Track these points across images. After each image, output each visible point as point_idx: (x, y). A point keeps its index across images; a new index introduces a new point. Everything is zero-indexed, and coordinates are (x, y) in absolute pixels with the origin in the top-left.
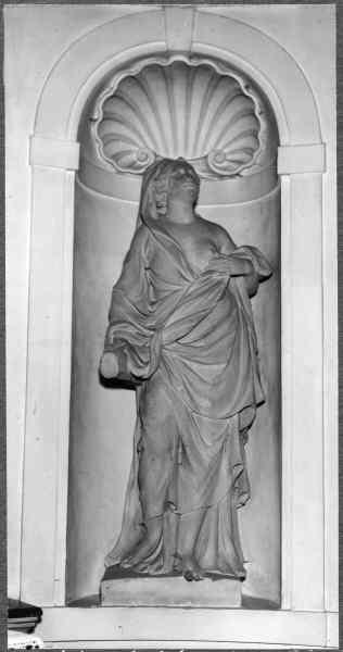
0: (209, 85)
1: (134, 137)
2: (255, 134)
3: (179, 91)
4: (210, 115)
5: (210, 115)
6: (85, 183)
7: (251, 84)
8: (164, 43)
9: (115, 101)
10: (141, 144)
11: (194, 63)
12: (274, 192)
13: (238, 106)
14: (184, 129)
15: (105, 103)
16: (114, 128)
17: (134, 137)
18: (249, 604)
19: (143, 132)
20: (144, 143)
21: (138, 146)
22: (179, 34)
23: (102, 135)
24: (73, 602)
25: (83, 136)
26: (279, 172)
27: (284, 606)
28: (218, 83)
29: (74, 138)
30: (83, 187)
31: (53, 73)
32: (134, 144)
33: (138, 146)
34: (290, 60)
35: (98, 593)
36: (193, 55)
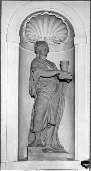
0: (42, 19)
1: (32, 31)
2: (67, 34)
3: (52, 23)
4: (58, 29)
5: (58, 29)
6: (22, 47)
7: (67, 21)
8: (42, 9)
9: (28, 23)
10: (34, 33)
11: (50, 14)
12: (73, 48)
13: (63, 27)
14: (45, 32)
15: (27, 24)
16: (28, 29)
17: (32, 31)
18: (69, 159)
19: (34, 30)
20: (35, 33)
21: (33, 33)
22: (47, 6)
23: (26, 35)
24: (20, 160)
25: (21, 34)
26: (74, 44)
27: (76, 159)
28: (57, 20)
29: (18, 34)
30: (22, 48)
31: (14, 16)
32: (32, 32)
33: (33, 33)
34: (77, 15)
35: (27, 157)
36: (50, 12)
